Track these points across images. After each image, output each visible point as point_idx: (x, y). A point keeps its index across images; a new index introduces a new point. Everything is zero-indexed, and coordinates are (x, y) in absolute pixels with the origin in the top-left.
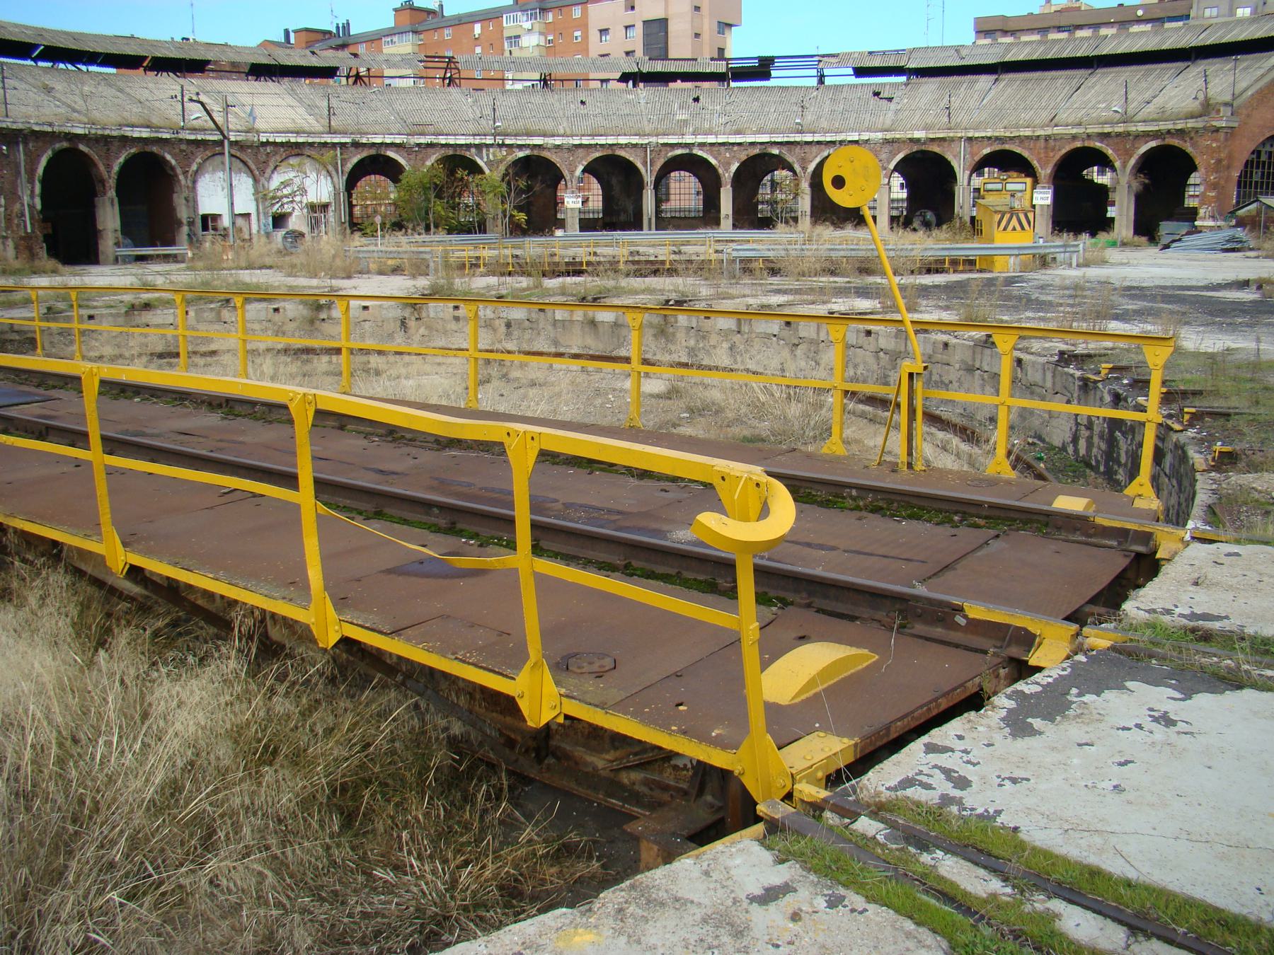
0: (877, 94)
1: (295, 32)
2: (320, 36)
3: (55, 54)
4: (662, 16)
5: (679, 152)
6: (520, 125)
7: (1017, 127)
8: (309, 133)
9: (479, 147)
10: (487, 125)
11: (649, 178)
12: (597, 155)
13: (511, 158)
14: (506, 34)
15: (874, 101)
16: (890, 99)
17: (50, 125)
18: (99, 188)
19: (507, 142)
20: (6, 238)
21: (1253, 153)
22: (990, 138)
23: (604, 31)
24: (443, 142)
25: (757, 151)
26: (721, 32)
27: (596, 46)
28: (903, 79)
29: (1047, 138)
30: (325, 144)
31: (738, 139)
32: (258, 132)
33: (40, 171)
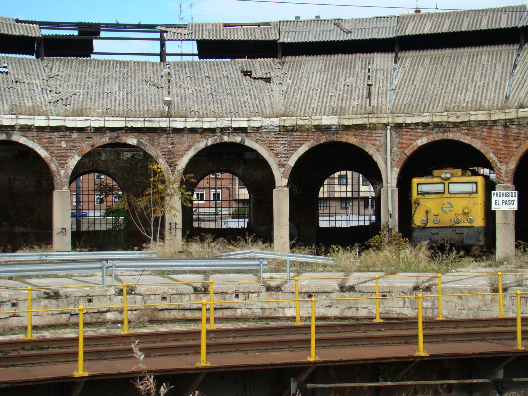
15: (246, 81)
22: (425, 125)
29: (507, 124)
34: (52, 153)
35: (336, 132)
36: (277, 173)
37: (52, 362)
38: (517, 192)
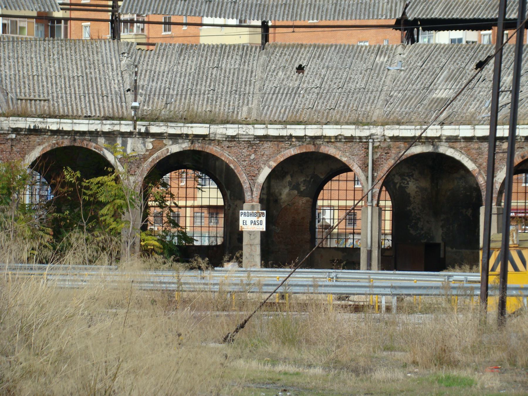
5: (417, 149)
6: (179, 106)
9: (110, 136)
12: (293, 152)
19: (154, 129)
24: (54, 127)
34: (480, 165)
38: (265, 212)
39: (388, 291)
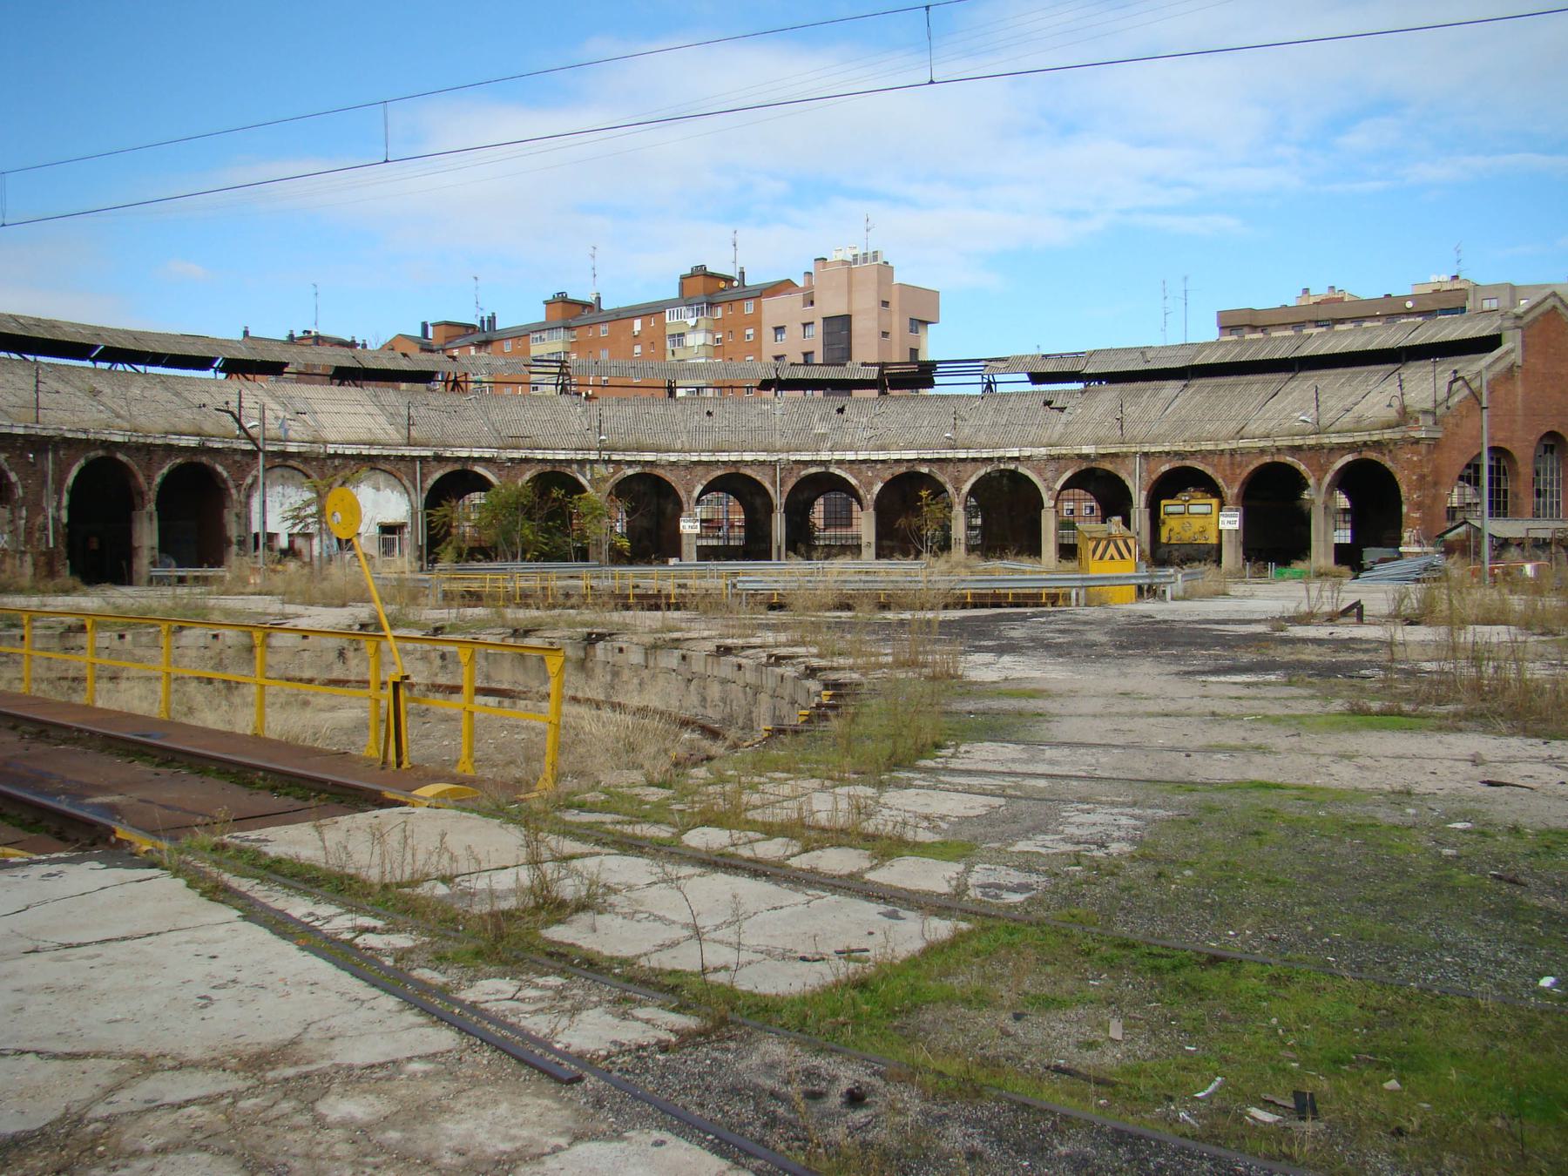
0: (1048, 403)
1: (434, 325)
2: (463, 331)
3: (114, 355)
4: (843, 311)
6: (631, 440)
7: (1198, 440)
8: (384, 445)
10: (593, 438)
11: (779, 500)
12: (719, 473)
13: (620, 476)
14: (669, 332)
15: (1044, 412)
16: (1062, 409)
17: (85, 431)
18: (137, 500)
19: (615, 457)
20: (24, 553)
21: (1468, 466)
22: (1168, 453)
23: (779, 330)
25: (903, 469)
26: (914, 330)
27: (770, 347)
28: (1080, 386)
29: (1233, 452)
30: (403, 458)
31: (882, 456)
32: (325, 443)
33: (70, 481)
35: (1095, 460)
36: (1045, 496)
37: (1371, 794)
39: (1078, 584)
